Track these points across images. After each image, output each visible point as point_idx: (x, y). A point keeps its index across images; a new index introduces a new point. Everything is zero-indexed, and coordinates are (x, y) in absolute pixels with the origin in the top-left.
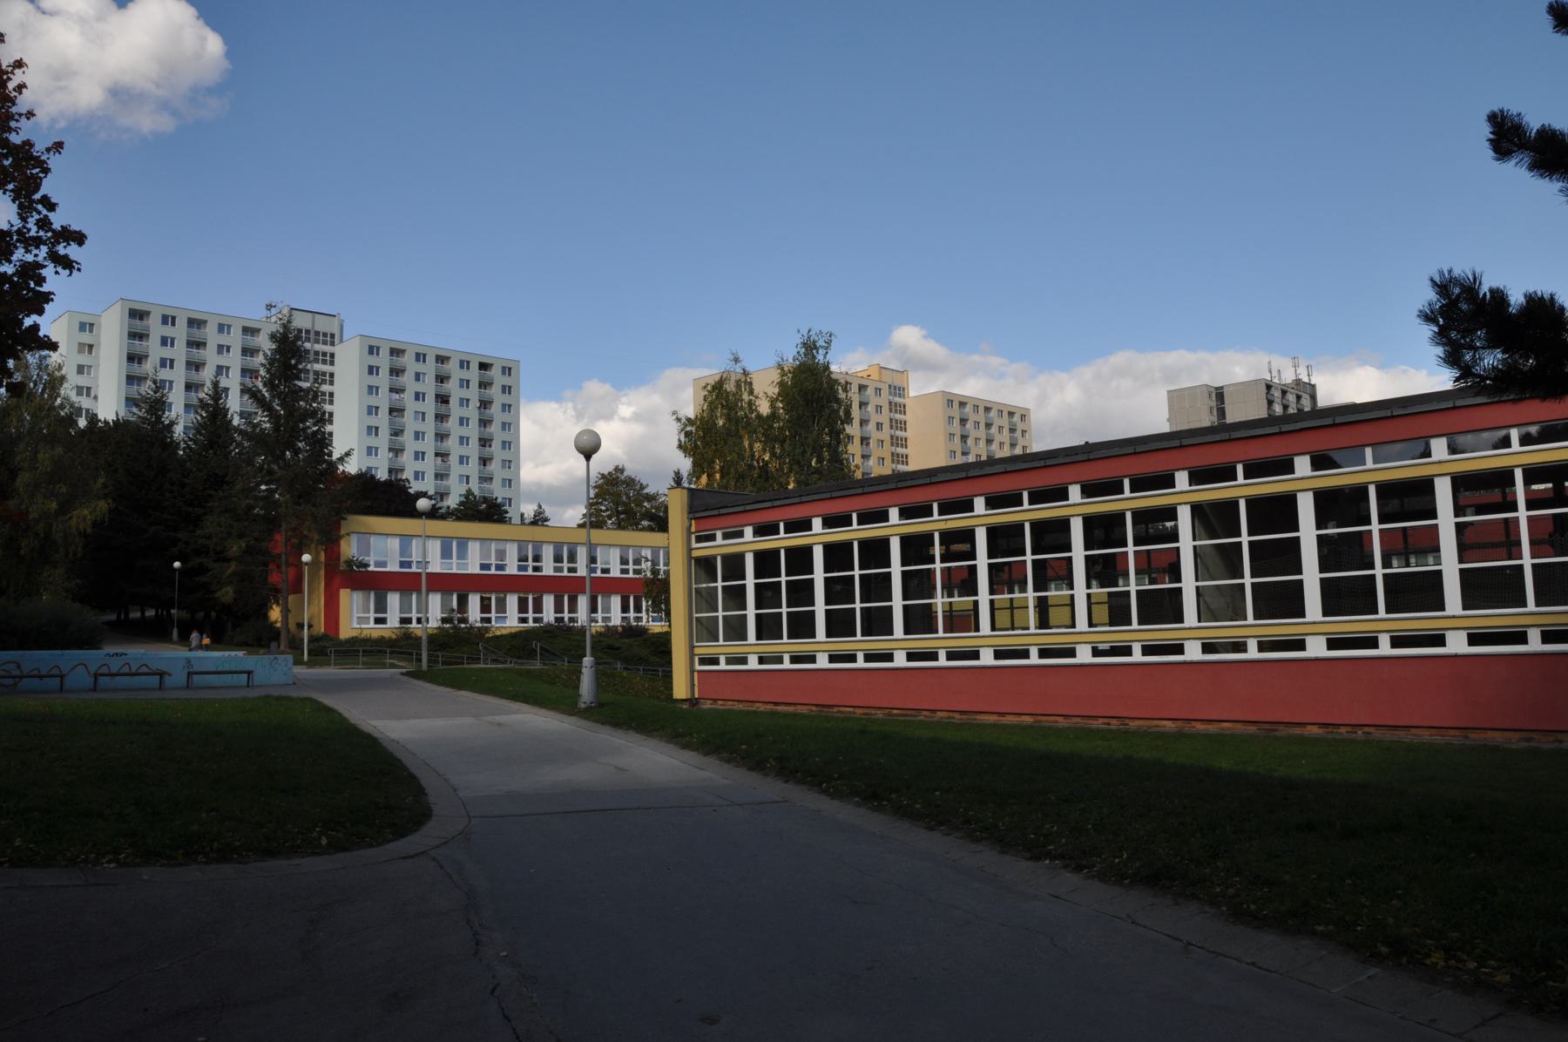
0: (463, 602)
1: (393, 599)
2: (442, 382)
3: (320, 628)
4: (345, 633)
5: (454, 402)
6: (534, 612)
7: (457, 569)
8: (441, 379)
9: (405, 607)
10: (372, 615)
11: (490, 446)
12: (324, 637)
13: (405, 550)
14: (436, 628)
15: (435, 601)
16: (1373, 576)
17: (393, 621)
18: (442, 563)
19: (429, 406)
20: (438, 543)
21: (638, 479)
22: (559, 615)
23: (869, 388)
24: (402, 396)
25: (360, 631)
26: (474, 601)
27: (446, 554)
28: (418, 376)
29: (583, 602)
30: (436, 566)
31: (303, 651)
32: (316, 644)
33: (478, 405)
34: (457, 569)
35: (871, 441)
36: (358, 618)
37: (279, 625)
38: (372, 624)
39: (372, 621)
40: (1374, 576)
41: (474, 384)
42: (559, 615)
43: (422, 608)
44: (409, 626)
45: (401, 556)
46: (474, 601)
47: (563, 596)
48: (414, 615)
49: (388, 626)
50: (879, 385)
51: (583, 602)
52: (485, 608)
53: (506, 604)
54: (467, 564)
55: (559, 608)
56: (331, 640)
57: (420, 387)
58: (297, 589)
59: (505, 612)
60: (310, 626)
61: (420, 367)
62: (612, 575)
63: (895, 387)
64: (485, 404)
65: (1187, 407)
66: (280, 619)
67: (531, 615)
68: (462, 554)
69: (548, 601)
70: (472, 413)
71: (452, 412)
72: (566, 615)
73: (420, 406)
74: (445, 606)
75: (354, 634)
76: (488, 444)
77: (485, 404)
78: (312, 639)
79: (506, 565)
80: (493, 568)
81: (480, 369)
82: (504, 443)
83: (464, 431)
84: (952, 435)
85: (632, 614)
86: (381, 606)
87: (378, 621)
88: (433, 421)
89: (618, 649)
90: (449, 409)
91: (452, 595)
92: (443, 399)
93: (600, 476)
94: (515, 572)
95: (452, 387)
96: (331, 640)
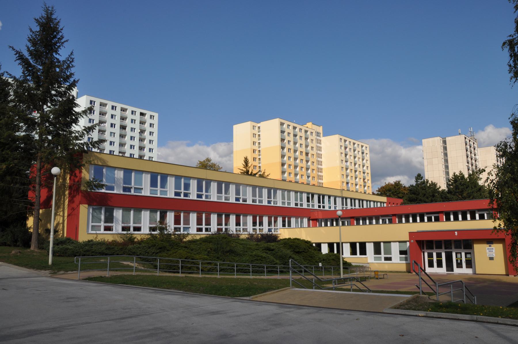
0: (163, 217)
1: (118, 214)
2: (123, 120)
3: (64, 233)
4: (83, 237)
5: (128, 129)
6: (206, 225)
7: (161, 195)
8: (123, 119)
9: (125, 219)
10: (102, 224)
11: (144, 150)
12: (68, 241)
13: (127, 179)
14: (148, 234)
15: (145, 215)
16: (184, 224)
17: (117, 228)
18: (151, 190)
19: (117, 130)
20: (149, 176)
21: (217, 164)
22: (219, 227)
23: (308, 132)
24: (105, 124)
25: (95, 236)
26: (170, 217)
27: (154, 184)
28: (112, 116)
29: (233, 219)
30: (146, 192)
31: (49, 252)
32: (60, 246)
33: (139, 131)
34: (161, 195)
35: (309, 154)
36: (92, 226)
37: (31, 230)
38: (102, 231)
39: (102, 228)
40: (184, 225)
41: (137, 122)
42: (219, 227)
43: (138, 220)
44: (422, 249)
45: (124, 183)
46: (170, 217)
47: (222, 215)
48: (132, 225)
49: (114, 232)
50: (312, 131)
51: (233, 219)
52: (177, 221)
53: (189, 220)
54: (167, 191)
55: (219, 223)
56: (73, 243)
57: (113, 121)
58: (47, 205)
59: (189, 225)
60: (56, 231)
61: (113, 112)
62: (248, 203)
63: (317, 132)
64: (142, 132)
65: (431, 146)
66: (32, 226)
67: (204, 227)
68: (164, 184)
69: (214, 218)
70: (136, 134)
71: (127, 134)
72: (224, 227)
73: (112, 130)
74: (152, 220)
75: (90, 238)
76: (143, 149)
77: (142, 132)
78: (57, 242)
79: (190, 193)
80: (182, 195)
81: (140, 115)
82: (150, 149)
83: (132, 143)
84: (341, 153)
85: (258, 227)
86: (109, 219)
87: (107, 229)
88: (119, 137)
89: (273, 250)
90: (126, 132)
91: (157, 212)
92: (123, 127)
93: (199, 162)
94: (195, 198)
95: (128, 122)
96: (73, 243)
